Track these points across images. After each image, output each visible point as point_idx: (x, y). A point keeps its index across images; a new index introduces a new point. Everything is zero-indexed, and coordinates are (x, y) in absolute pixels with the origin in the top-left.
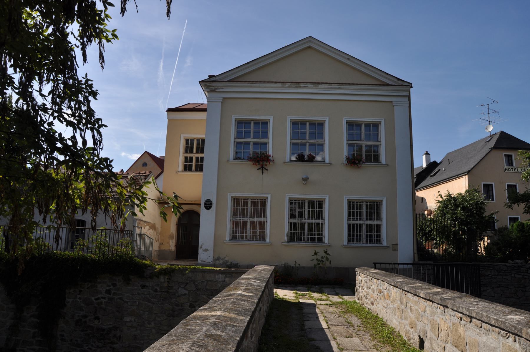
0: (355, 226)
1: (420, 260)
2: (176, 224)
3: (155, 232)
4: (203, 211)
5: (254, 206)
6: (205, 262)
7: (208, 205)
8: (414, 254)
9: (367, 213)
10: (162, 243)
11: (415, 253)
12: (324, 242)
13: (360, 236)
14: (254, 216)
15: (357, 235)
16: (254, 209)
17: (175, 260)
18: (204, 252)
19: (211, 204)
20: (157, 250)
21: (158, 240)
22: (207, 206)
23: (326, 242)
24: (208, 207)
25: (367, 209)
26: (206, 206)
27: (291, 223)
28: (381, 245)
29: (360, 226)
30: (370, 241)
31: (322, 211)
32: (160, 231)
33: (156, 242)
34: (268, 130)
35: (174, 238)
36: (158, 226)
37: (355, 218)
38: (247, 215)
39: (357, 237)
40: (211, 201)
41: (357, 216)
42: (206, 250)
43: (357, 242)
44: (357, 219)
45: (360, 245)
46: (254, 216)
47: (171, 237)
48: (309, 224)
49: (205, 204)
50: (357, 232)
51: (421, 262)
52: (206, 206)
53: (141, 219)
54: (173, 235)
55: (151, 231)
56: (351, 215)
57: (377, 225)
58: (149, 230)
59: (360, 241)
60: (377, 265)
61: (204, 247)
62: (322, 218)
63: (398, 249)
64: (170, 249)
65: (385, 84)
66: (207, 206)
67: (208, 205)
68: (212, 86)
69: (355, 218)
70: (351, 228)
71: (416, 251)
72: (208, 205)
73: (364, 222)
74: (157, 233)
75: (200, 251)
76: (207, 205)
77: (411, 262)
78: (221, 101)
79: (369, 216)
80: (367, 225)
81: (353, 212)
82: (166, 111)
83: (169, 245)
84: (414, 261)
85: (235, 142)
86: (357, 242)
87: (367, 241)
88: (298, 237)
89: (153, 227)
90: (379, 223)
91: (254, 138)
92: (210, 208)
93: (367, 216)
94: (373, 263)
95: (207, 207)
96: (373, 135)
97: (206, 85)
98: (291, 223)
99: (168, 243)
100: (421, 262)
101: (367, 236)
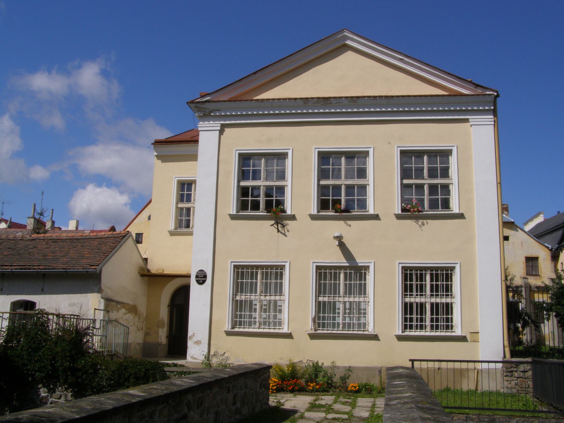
0: (415, 305)
1: (513, 354)
2: (169, 306)
3: (137, 319)
4: (195, 288)
5: (267, 279)
6: (196, 359)
7: (201, 278)
8: (504, 347)
9: (432, 286)
10: (148, 333)
11: (505, 345)
12: (368, 330)
13: (421, 320)
14: (266, 292)
15: (417, 318)
16: (266, 283)
17: (166, 357)
18: (195, 346)
19: (205, 276)
20: (141, 344)
21: (142, 329)
22: (200, 279)
23: (370, 330)
24: (201, 282)
25: (432, 280)
26: (197, 279)
27: (406, 304)
28: (453, 334)
29: (422, 306)
30: (411, 327)
31: (451, 285)
32: (145, 315)
33: (138, 331)
34: (286, 168)
35: (166, 325)
36: (142, 308)
37: (414, 293)
38: (256, 292)
39: (417, 321)
40: (205, 273)
41: (417, 291)
42: (198, 343)
43: (417, 329)
44: (417, 295)
45: (418, 333)
46: (266, 292)
47: (160, 324)
48: (432, 304)
49: (197, 277)
50: (417, 314)
51: (514, 360)
52: (197, 279)
53: (113, 299)
54: (164, 321)
55: (130, 316)
56: (407, 289)
57: (447, 304)
58: (125, 314)
59: (421, 327)
60: (415, 362)
61: (195, 339)
62: (365, 294)
63: (479, 340)
64: (160, 341)
65: (452, 93)
66: (200, 279)
67: (201, 278)
68: (205, 108)
69: (414, 293)
70: (407, 308)
71: (506, 343)
72: (201, 278)
73: (428, 300)
74: (139, 318)
75: (190, 343)
76: (199, 278)
77: (501, 360)
78: (219, 128)
79: (435, 289)
80: (432, 304)
81: (411, 285)
82: (152, 144)
83: (158, 336)
84: (505, 357)
85: (240, 187)
86: (417, 329)
87: (432, 327)
88: (328, 320)
89: (133, 309)
90: (449, 300)
91: (267, 179)
92: (204, 282)
93: (432, 291)
94: (410, 360)
95: (200, 280)
96: (274, 172)
97: (196, 107)
98: (406, 304)
99: (157, 332)
100: (514, 360)
101: (432, 320)
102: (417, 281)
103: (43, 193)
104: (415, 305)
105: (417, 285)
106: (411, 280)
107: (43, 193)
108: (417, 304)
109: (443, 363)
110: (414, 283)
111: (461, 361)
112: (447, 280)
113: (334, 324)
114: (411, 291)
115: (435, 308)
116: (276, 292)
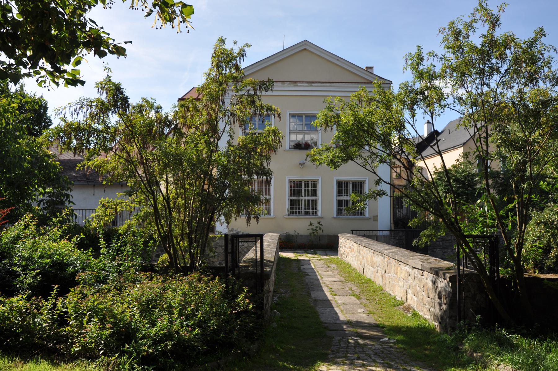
0: (343, 202)
8: (391, 223)
23: (319, 215)
27: (291, 200)
28: (364, 217)
37: (343, 195)
41: (345, 194)
44: (345, 196)
48: (305, 200)
56: (339, 193)
62: (316, 195)
69: (343, 195)
71: (392, 222)
80: (305, 200)
81: (342, 190)
102: (345, 188)
103: (188, 32)
104: (343, 202)
105: (345, 190)
106: (342, 187)
107: (188, 32)
108: (345, 201)
109: (374, 232)
110: (343, 189)
111: (382, 231)
112: (314, 187)
113: (299, 212)
114: (342, 193)
115: (307, 202)
116: (266, 194)
